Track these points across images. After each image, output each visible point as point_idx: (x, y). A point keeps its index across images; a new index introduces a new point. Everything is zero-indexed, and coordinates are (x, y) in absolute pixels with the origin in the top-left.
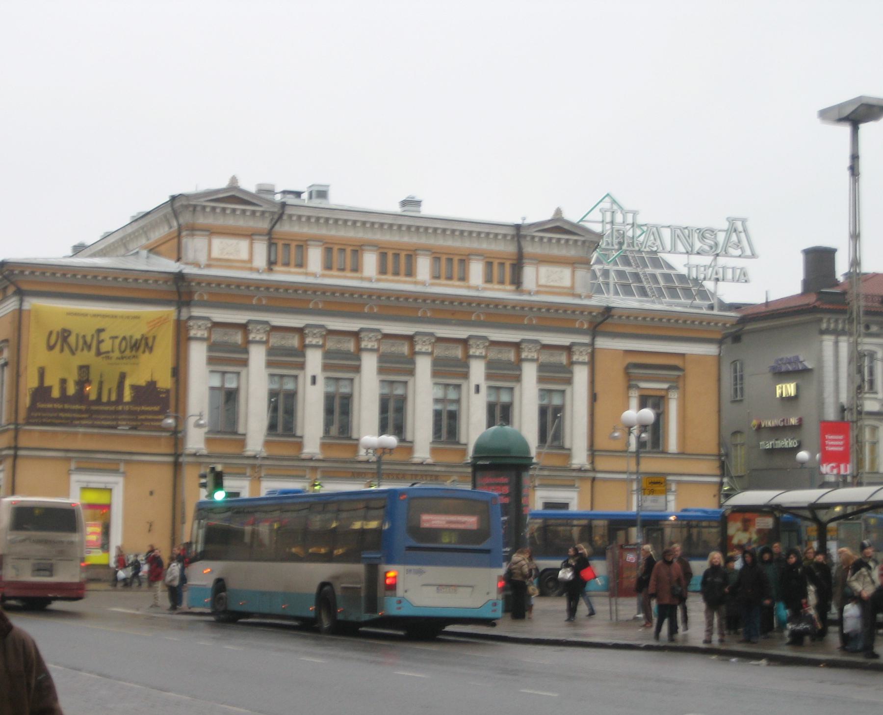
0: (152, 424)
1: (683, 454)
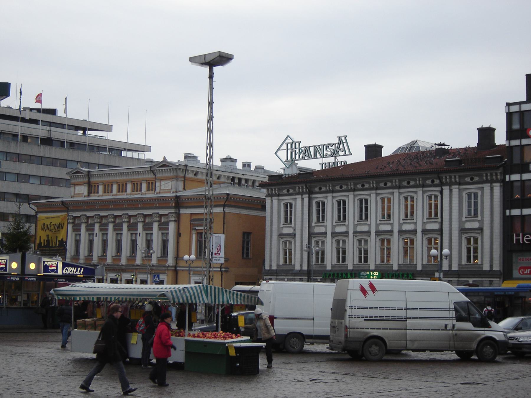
0: (387, 266)
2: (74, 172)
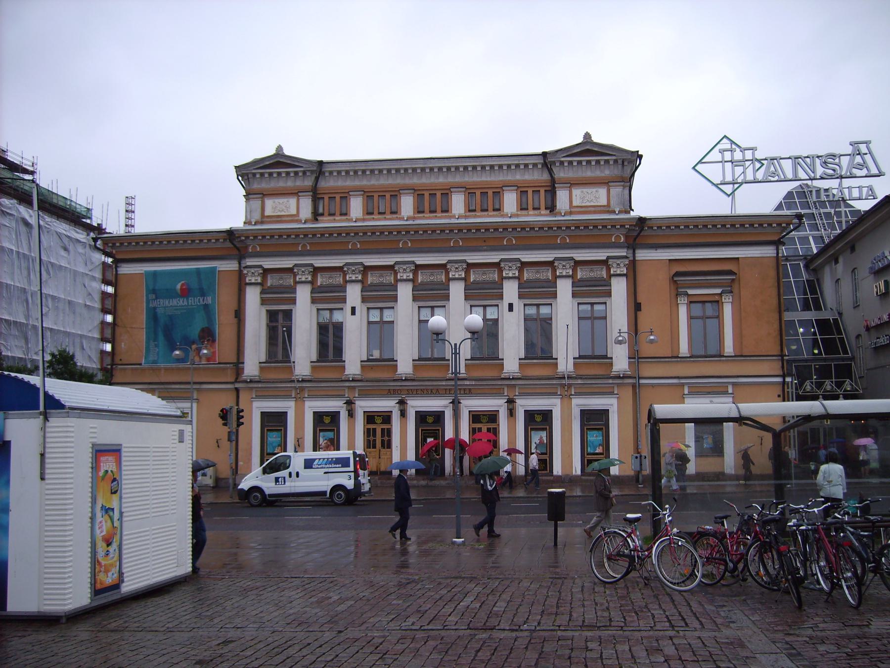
1: (740, 356)
2: (268, 163)
